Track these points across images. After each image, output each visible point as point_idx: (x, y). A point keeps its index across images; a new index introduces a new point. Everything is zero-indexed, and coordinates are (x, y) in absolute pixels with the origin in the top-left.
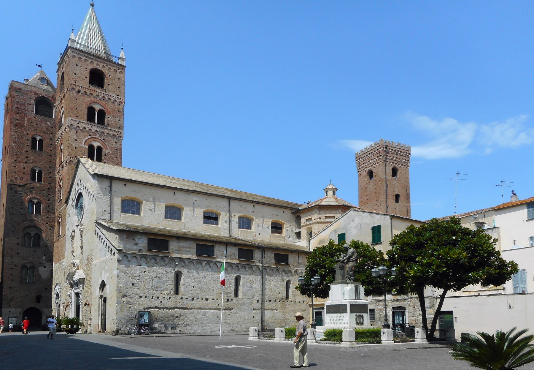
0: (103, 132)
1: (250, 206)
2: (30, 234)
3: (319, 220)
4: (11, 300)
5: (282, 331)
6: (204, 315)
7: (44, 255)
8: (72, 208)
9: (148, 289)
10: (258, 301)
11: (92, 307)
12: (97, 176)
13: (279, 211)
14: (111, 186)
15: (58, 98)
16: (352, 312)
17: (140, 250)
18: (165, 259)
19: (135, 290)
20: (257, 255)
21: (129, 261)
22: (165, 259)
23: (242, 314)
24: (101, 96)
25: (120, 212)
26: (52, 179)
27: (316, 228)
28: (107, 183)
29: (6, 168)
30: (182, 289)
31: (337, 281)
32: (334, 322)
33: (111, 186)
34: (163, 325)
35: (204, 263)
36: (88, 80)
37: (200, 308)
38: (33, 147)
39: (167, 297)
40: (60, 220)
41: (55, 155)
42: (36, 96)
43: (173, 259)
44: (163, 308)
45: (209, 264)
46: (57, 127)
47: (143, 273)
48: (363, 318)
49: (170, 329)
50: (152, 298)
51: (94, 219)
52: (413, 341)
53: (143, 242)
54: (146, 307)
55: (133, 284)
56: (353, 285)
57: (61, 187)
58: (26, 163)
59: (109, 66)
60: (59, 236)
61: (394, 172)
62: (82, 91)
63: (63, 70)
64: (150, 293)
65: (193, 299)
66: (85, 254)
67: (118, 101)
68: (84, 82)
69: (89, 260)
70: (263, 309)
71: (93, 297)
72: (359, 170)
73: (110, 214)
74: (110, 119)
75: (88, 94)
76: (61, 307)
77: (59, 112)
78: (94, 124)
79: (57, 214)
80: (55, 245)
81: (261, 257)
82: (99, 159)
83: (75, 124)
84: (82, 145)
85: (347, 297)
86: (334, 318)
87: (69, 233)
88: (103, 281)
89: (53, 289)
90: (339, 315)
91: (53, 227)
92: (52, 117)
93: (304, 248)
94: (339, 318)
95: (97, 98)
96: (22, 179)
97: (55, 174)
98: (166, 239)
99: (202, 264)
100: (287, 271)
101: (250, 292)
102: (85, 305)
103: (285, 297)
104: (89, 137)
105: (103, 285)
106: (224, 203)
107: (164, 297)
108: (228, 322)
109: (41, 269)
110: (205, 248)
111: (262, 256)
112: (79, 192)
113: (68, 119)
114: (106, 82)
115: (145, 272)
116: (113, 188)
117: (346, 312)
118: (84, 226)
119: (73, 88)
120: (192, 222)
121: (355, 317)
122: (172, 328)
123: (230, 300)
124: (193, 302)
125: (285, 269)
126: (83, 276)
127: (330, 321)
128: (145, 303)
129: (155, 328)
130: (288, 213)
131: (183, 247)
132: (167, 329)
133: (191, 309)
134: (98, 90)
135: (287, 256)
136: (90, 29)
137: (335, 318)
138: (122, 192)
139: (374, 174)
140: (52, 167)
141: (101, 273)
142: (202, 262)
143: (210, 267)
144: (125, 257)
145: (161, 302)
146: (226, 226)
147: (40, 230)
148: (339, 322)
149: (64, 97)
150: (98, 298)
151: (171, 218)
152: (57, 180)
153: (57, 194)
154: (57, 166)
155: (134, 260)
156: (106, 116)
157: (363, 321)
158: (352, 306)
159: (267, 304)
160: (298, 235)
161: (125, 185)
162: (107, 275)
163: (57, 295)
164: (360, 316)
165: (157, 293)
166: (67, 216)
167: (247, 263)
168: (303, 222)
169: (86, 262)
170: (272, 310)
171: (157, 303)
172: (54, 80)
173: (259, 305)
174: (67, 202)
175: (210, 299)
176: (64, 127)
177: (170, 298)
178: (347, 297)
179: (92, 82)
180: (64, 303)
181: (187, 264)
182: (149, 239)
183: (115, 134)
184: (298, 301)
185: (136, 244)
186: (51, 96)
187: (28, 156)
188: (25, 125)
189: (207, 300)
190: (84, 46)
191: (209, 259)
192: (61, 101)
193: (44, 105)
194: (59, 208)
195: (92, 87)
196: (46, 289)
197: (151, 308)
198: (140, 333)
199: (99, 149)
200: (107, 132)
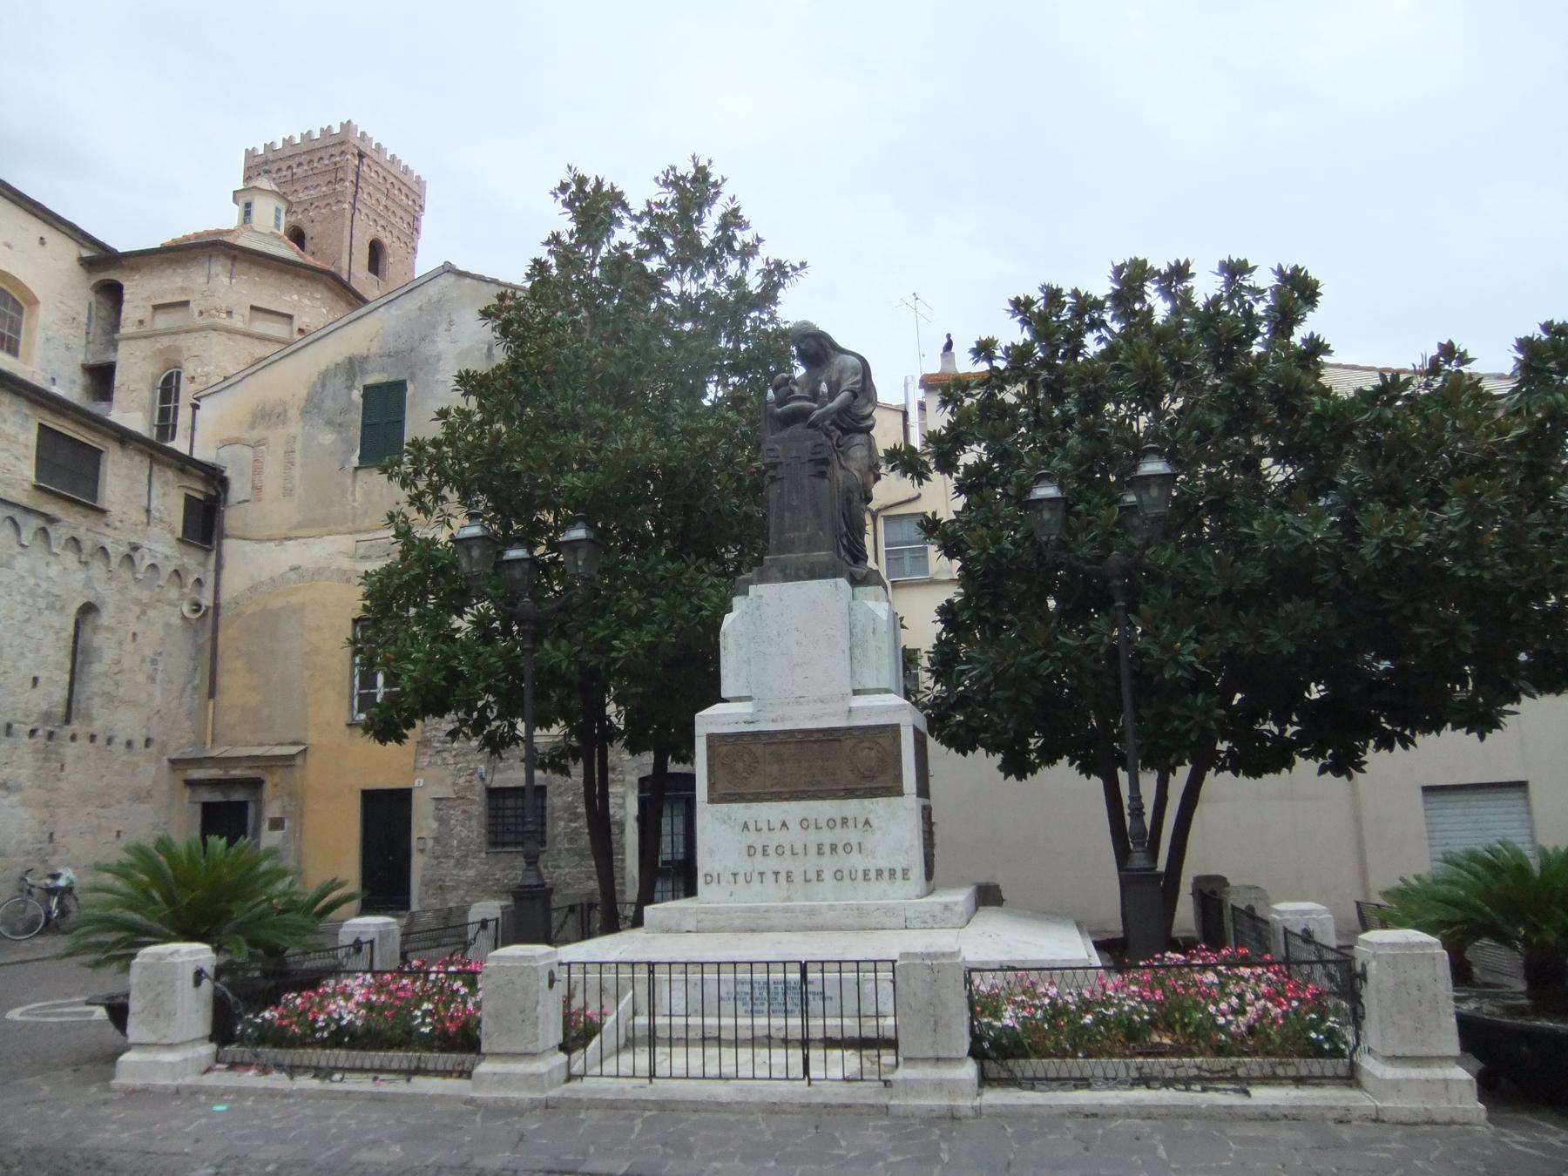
27: (209, 359)
31: (797, 556)
32: (783, 865)
86: (779, 837)
94: (827, 837)
100: (87, 546)
103: (60, 710)
117: (900, 793)
125: (81, 534)
127: (745, 865)
137: (795, 836)
148: (828, 864)
168: (138, 315)
184: (121, 739)
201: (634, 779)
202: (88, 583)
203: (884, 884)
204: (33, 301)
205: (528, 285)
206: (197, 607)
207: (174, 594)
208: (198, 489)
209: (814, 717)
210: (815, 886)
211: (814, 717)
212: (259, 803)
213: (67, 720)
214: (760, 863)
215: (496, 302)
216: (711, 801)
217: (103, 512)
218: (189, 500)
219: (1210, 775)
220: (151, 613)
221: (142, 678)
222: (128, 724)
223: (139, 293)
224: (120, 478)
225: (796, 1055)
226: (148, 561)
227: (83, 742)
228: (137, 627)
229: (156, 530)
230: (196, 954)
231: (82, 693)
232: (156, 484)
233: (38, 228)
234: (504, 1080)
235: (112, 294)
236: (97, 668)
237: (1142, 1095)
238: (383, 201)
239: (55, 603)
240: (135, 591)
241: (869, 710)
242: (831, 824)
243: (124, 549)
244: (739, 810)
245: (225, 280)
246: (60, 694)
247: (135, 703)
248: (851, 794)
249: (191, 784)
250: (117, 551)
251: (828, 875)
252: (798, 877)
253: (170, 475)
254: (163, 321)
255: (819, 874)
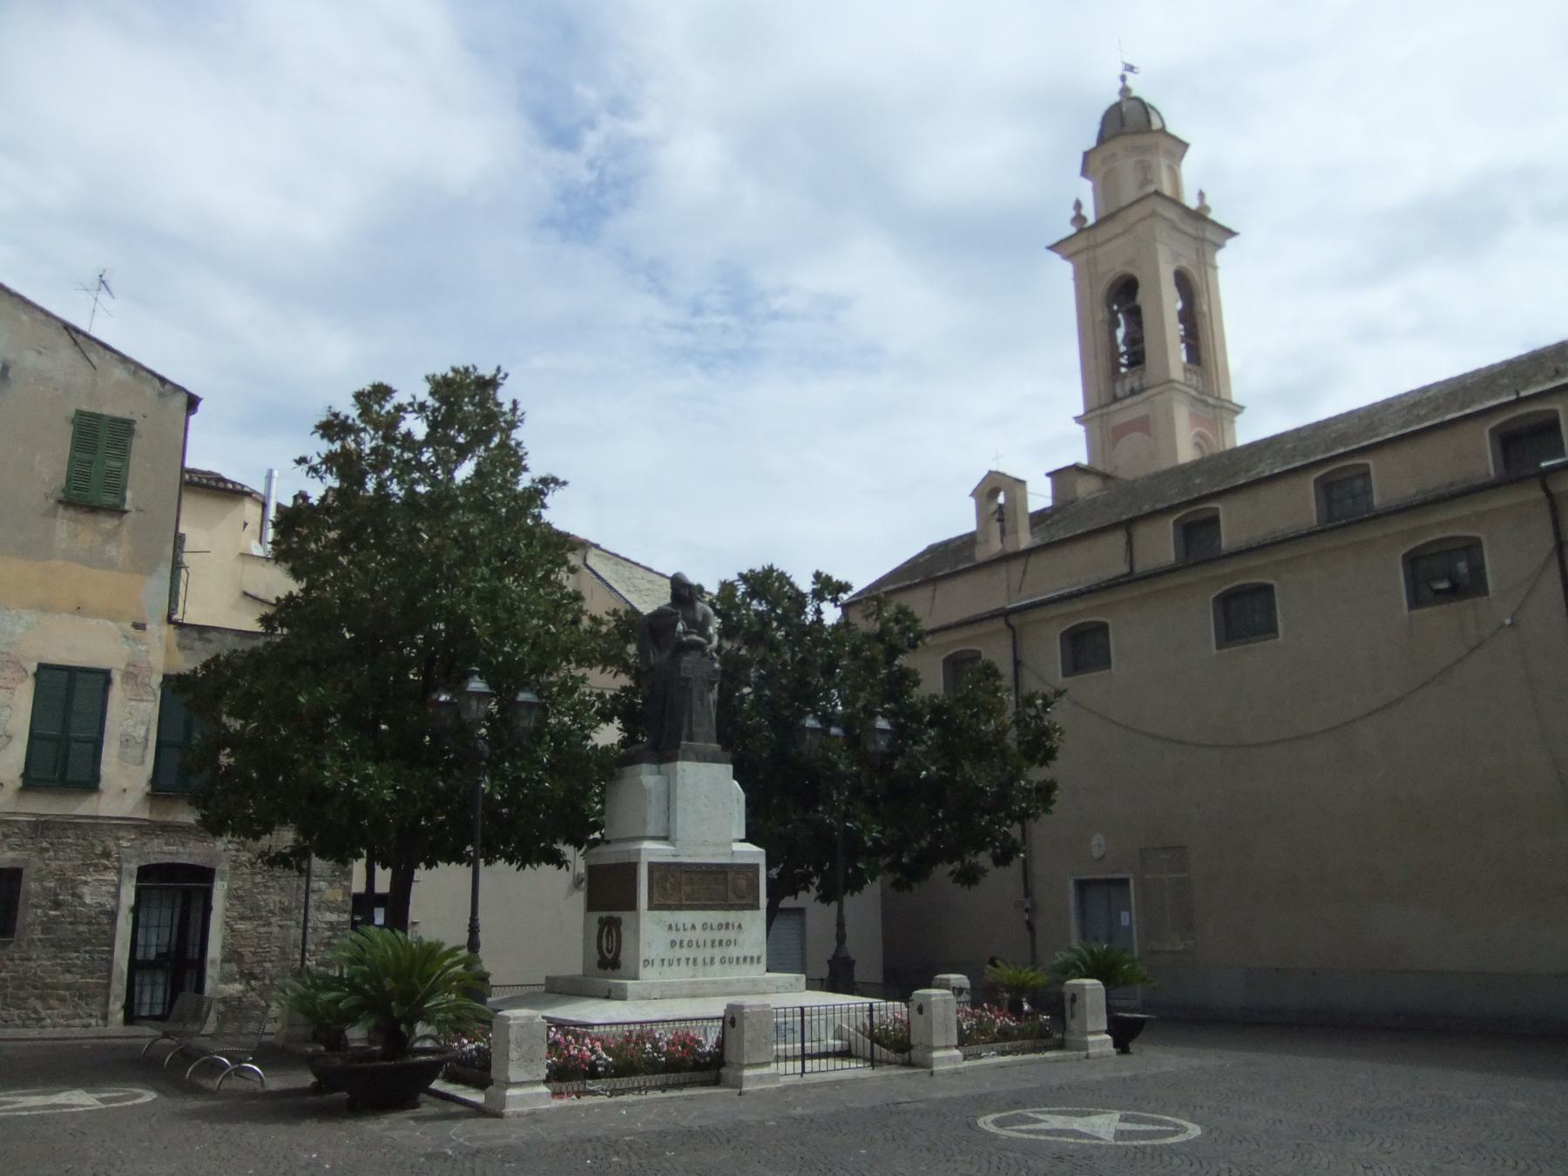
94: (719, 935)
137: (699, 934)
148: (718, 952)
201: (133, 866)
203: (747, 966)
205: (513, 443)
209: (713, 856)
210: (709, 968)
211: (713, 856)
215: (805, 585)
216: (650, 908)
219: (421, 873)
225: (798, 1064)
234: (761, 1078)
237: (1020, 1057)
242: (720, 926)
244: (667, 916)
248: (731, 907)
251: (717, 960)
252: (700, 961)
255: (712, 960)
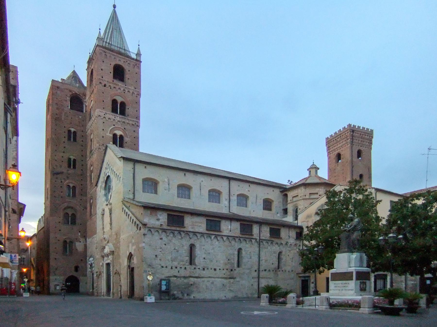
0: (124, 122)
1: (246, 185)
2: (69, 215)
3: (304, 197)
4: (56, 269)
5: (294, 298)
6: (212, 283)
7: (80, 232)
8: (102, 190)
9: (168, 260)
10: (256, 271)
11: (121, 276)
12: (126, 159)
13: (270, 190)
14: (134, 169)
15: (88, 93)
16: (357, 279)
17: (161, 225)
18: (182, 233)
19: (158, 261)
20: (256, 229)
21: (153, 235)
22: (182, 233)
23: (243, 282)
24: (122, 89)
25: (142, 191)
26: (84, 166)
27: (301, 205)
28: (130, 165)
29: (49, 157)
30: (197, 261)
32: (339, 288)
33: (134, 169)
34: (180, 292)
35: (213, 237)
36: (112, 74)
37: (210, 277)
38: (69, 139)
39: (183, 268)
40: (91, 201)
41: (86, 145)
42: (71, 93)
43: (187, 233)
44: (180, 277)
45: (217, 238)
46: (88, 119)
47: (164, 246)
48: (366, 284)
49: (186, 295)
50: (172, 268)
51: (121, 197)
52: (358, 310)
53: (163, 218)
54: (167, 276)
55: (156, 256)
56: (358, 254)
57: (92, 172)
58: (64, 152)
59: (128, 62)
60: (91, 214)
61: (359, 154)
62: (107, 86)
63: (92, 67)
64: (169, 264)
65: (204, 269)
66: (114, 230)
67: (136, 93)
68: (109, 77)
69: (117, 234)
70: (259, 277)
71: (122, 267)
72: (329, 153)
73: (134, 193)
74: (129, 110)
75: (112, 87)
76: (95, 275)
77: (89, 106)
78: (117, 115)
79: (89, 196)
80: (88, 223)
81: (258, 231)
82: (121, 146)
83: (102, 114)
84: (108, 134)
85: (353, 264)
87: (99, 212)
88: (130, 253)
89: (88, 260)
90: (344, 282)
91: (86, 208)
92: (82, 111)
93: (291, 223)
95: (119, 91)
96: (61, 166)
97: (86, 161)
98: (182, 215)
99: (211, 238)
101: (249, 263)
102: (115, 274)
103: (277, 267)
104: (113, 127)
105: (130, 256)
106: (225, 183)
107: (181, 268)
108: (232, 289)
109: (77, 244)
110: (214, 221)
111: (260, 229)
112: (107, 175)
113: (96, 111)
114: (127, 76)
115: (165, 245)
116: (136, 170)
118: (113, 205)
119: (100, 83)
120: (200, 201)
121: (359, 283)
122: (188, 295)
123: (233, 270)
124: (204, 272)
126: (113, 249)
128: (166, 273)
129: (174, 295)
130: (277, 191)
131: (196, 222)
132: (183, 295)
133: (203, 277)
134: (120, 84)
135: (279, 230)
136: (113, 29)
138: (143, 173)
139: (342, 157)
140: (84, 156)
141: (129, 246)
142: (211, 236)
143: (218, 240)
144: (149, 232)
145: (179, 271)
146: (227, 203)
147: (75, 210)
148: (344, 288)
149: (93, 91)
150: (126, 268)
151: (182, 197)
152: (89, 166)
153: (88, 179)
154: (88, 154)
155: (156, 234)
156: (127, 107)
157: (366, 286)
158: (358, 273)
159: (262, 274)
160: (285, 211)
161: (145, 167)
162: (134, 247)
163: (91, 265)
164: (363, 282)
165: (175, 264)
166: (98, 197)
167: (247, 236)
169: (115, 237)
170: (267, 278)
171: (175, 272)
172: (84, 78)
173: (256, 274)
174: (96, 185)
175: (218, 269)
176: (93, 119)
177: (185, 268)
178: (353, 264)
179: (115, 77)
180: (97, 272)
181: (199, 237)
182: (169, 215)
183: (134, 123)
184: (287, 270)
185: (158, 220)
186: (82, 93)
187: (65, 146)
188: (63, 119)
189: (215, 270)
190: (109, 43)
191: (217, 233)
192: (90, 96)
193: (77, 102)
194: (90, 191)
195: (115, 81)
196: (82, 260)
197: (171, 277)
198: (161, 299)
199: (121, 137)
200: (127, 121)
202: (280, 248)
204: (273, 201)
206: (299, 249)
207: (295, 248)
208: (298, 231)
212: (310, 280)
213: (278, 268)
214: (336, 288)
217: (281, 238)
218: (297, 233)
220: (291, 252)
221: (290, 261)
222: (288, 268)
223: (291, 194)
224: (284, 233)
226: (290, 244)
227: (281, 272)
228: (289, 254)
229: (291, 239)
230: (267, 295)
231: (281, 265)
232: (290, 232)
233: (272, 189)
235: (286, 195)
236: (282, 261)
238: (361, 140)
239: (275, 253)
240: (288, 249)
241: (350, 270)
243: (285, 243)
245: (304, 190)
246: (276, 265)
247: (289, 265)
249: (300, 277)
250: (284, 243)
253: (293, 230)
254: (295, 199)
